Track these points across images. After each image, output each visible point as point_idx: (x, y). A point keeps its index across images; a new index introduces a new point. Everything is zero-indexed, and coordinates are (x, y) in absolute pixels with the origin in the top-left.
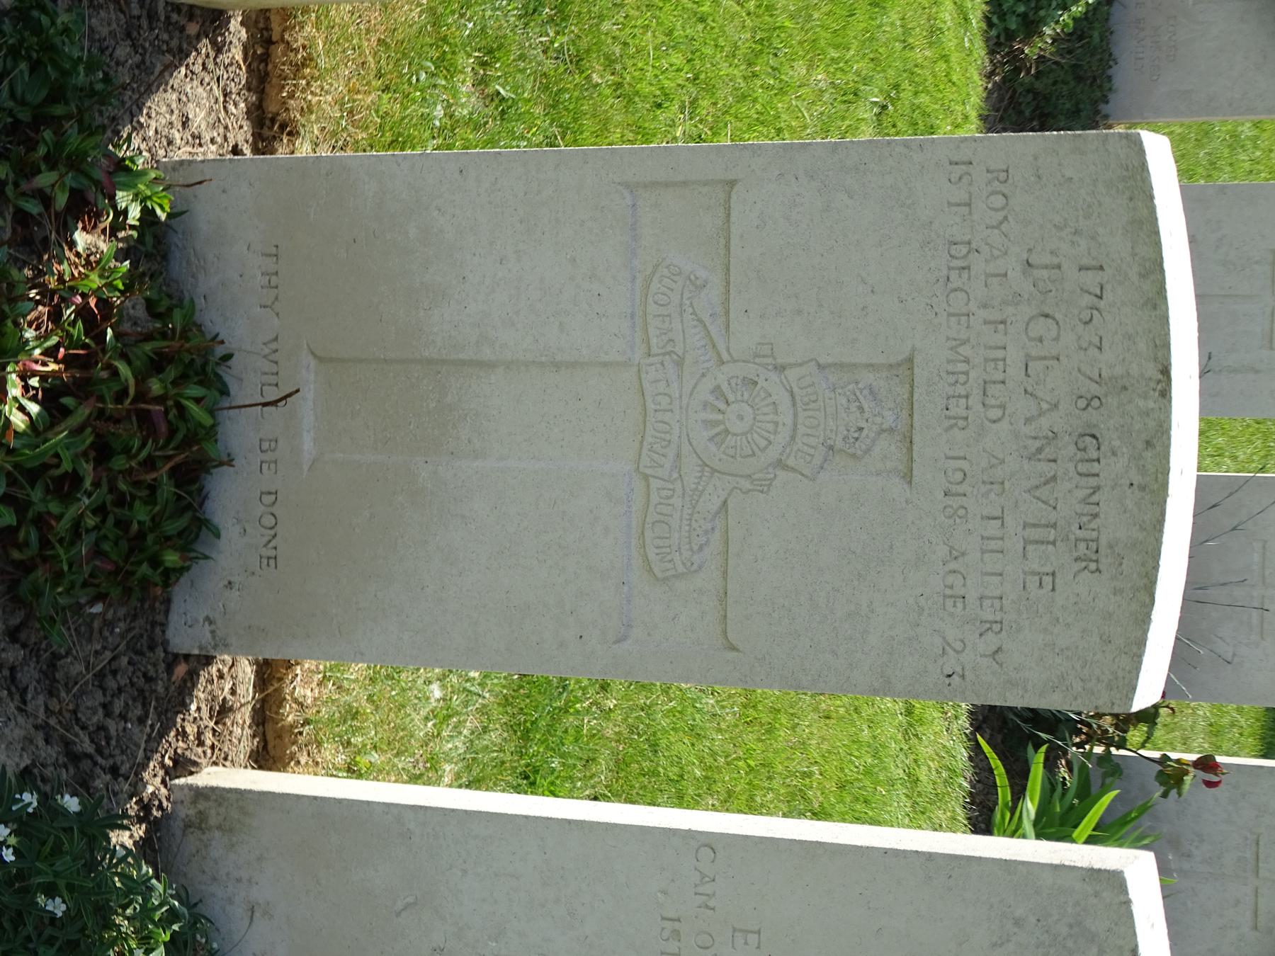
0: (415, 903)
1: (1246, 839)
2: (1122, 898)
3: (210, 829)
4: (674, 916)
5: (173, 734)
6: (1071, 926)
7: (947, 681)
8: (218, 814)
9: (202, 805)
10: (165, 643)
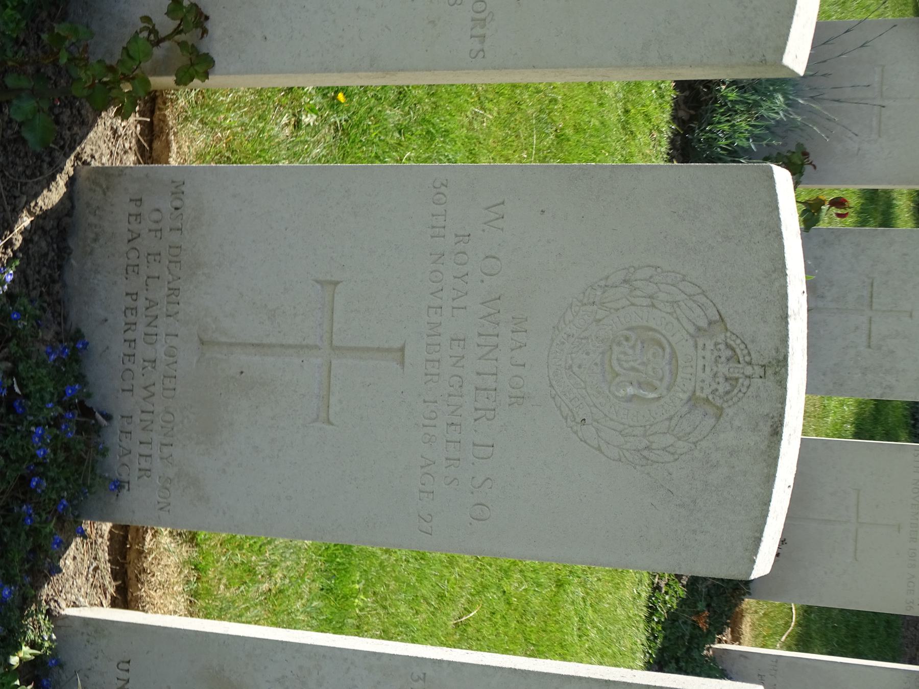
1: (864, 282)
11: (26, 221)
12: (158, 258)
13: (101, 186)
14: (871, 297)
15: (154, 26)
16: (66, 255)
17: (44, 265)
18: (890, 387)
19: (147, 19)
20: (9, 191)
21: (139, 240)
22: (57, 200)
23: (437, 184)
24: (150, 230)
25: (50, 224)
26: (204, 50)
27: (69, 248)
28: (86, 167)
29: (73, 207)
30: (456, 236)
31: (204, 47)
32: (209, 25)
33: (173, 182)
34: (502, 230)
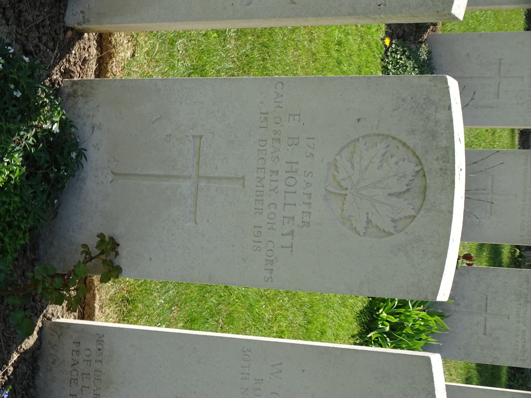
0: (160, 118)
1: (482, 297)
2: (446, 86)
3: (78, 96)
4: (266, 112)
5: (64, 60)
6: (425, 99)
7: (379, 7)
8: (82, 90)
9: (75, 87)
10: (64, 22)
11: (15, 356)
12: (88, 376)
13: (57, 333)
14: (486, 306)
15: (88, 250)
16: (37, 371)
17: (25, 379)
18: (496, 358)
19: (85, 246)
20: (6, 343)
21: (78, 365)
22: (32, 343)
23: (245, 350)
24: (84, 360)
25: (27, 356)
26: (116, 264)
27: (38, 366)
28: (49, 321)
29: (41, 343)
30: (255, 379)
31: (117, 262)
32: (119, 249)
33: (98, 334)
34: (281, 378)
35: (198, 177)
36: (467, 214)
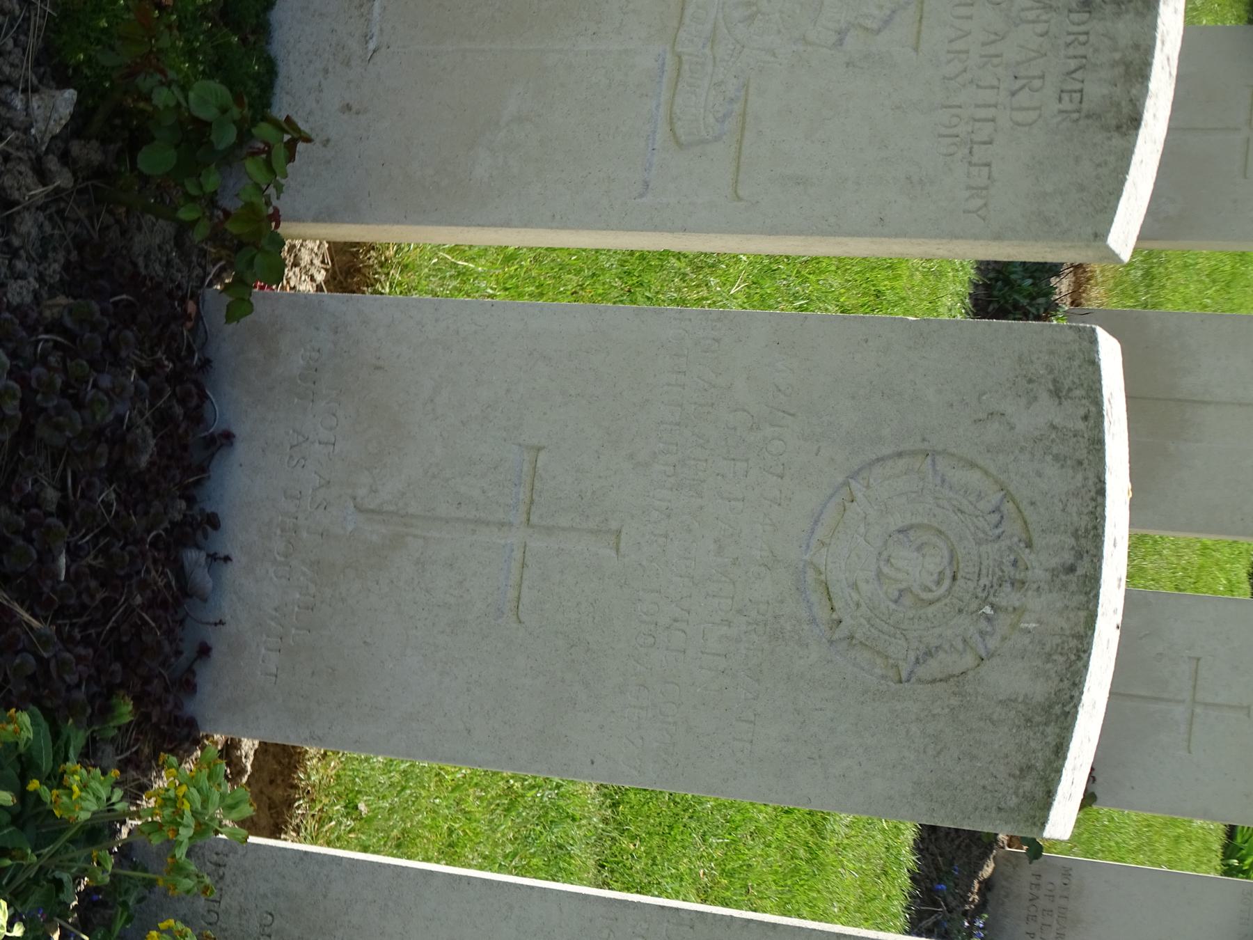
35: (1194, 701)
36: (1136, 544)
